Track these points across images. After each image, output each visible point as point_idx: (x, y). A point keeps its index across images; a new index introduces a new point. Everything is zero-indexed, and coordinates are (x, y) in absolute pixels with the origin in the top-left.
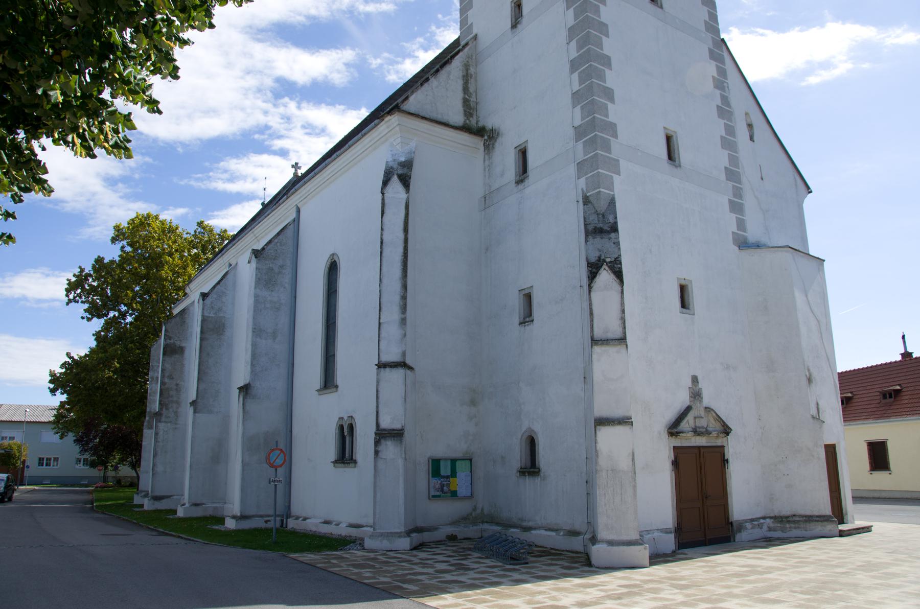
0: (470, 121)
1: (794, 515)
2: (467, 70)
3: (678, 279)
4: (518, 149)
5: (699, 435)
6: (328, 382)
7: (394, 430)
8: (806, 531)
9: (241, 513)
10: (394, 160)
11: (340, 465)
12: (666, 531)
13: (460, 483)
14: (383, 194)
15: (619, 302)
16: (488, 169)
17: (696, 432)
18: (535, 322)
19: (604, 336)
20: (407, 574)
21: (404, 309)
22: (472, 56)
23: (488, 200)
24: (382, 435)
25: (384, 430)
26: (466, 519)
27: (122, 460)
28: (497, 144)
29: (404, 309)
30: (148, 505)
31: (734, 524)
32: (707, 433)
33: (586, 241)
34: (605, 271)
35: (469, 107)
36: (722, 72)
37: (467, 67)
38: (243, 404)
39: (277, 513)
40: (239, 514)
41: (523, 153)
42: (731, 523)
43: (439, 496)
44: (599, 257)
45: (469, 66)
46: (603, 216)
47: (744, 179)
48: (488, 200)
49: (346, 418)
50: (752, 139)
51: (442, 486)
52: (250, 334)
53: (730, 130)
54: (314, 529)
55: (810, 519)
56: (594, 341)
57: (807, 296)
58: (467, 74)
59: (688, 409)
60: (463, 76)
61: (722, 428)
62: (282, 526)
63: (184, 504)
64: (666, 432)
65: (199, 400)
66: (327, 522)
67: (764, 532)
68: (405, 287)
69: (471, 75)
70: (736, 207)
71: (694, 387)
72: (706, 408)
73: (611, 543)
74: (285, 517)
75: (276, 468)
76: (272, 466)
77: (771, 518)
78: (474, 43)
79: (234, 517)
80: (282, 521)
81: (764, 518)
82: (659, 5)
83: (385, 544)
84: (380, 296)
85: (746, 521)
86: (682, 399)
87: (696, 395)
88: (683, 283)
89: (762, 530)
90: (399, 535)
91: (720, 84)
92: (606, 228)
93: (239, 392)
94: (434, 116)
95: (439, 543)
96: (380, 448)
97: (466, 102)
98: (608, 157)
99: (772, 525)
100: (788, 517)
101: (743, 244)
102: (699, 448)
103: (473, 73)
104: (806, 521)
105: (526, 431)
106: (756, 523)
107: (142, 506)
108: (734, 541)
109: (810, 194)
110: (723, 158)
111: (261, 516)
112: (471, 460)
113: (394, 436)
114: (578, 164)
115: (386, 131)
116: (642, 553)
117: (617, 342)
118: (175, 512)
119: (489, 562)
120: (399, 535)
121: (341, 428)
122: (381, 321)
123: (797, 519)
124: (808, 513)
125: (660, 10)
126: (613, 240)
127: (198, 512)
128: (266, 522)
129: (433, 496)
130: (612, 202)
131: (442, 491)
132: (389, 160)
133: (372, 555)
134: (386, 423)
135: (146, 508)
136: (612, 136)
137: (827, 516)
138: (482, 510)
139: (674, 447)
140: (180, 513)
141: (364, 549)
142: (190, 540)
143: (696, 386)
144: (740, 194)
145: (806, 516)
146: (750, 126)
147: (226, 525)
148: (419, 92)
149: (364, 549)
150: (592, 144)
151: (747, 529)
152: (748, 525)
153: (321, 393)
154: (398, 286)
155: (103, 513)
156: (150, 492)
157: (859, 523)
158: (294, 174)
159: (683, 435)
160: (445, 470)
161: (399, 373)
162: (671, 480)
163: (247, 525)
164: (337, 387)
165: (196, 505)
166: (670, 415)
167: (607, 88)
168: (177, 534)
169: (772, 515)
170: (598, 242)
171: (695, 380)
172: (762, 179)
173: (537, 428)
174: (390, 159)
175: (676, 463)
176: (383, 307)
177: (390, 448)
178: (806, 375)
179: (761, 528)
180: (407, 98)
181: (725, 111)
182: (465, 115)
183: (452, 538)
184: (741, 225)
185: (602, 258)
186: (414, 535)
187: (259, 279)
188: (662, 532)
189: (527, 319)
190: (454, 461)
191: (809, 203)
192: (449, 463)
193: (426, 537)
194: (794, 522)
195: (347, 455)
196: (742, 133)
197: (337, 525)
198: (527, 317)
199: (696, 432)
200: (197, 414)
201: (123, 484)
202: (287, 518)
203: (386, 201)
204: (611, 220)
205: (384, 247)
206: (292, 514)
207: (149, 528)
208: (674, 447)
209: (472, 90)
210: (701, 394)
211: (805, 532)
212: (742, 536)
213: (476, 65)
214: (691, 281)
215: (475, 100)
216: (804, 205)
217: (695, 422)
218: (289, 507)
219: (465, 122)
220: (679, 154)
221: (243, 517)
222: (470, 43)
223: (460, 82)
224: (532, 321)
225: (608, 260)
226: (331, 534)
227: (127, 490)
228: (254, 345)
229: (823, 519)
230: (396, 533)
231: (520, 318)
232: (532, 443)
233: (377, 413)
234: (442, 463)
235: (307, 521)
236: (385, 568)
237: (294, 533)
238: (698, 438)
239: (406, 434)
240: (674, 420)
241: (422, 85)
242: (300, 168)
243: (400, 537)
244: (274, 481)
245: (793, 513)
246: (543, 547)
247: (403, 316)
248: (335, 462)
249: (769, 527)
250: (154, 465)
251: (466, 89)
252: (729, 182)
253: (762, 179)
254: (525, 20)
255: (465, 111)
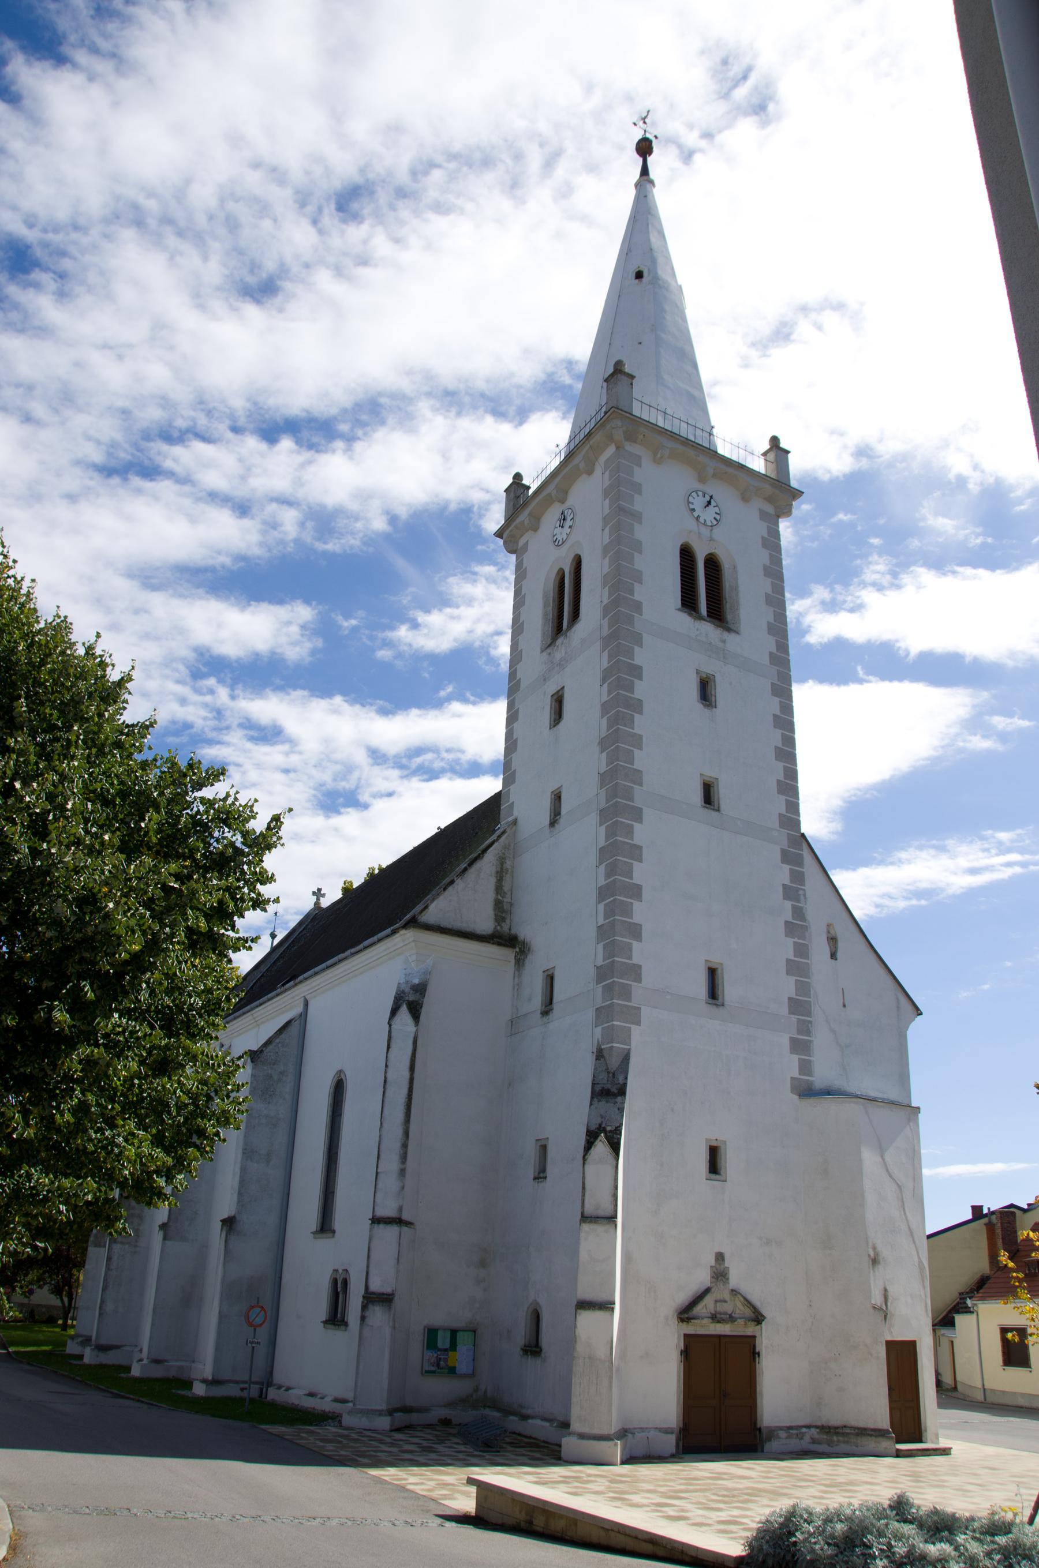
0: (502, 927)
1: (845, 1427)
2: (502, 864)
3: (707, 1140)
4: (547, 973)
5: (719, 1322)
6: (325, 1226)
7: (383, 1294)
8: (857, 1446)
9: (213, 1376)
10: (407, 982)
11: (330, 1326)
12: (667, 1431)
13: (461, 1359)
14: (390, 1026)
15: (613, 1178)
16: (517, 987)
17: (715, 1318)
18: (548, 1179)
19: (595, 1214)
20: (369, 1451)
21: (404, 1158)
22: (509, 845)
23: (515, 1025)
24: (371, 1298)
25: (373, 1293)
26: (464, 1402)
27: (40, 1281)
28: (527, 961)
29: (404, 1158)
30: (89, 1356)
31: (764, 1431)
32: (731, 1319)
33: (591, 1104)
34: (601, 1143)
35: (502, 910)
36: (798, 877)
37: (502, 860)
38: (226, 1241)
39: (253, 1379)
40: (210, 1378)
41: (550, 979)
42: (760, 1429)
43: (434, 1372)
44: (600, 1125)
45: (505, 858)
46: (614, 1074)
47: (815, 1009)
48: (515, 1025)
49: (340, 1271)
50: (833, 956)
51: (439, 1360)
52: (240, 1156)
53: (802, 950)
54: (296, 1402)
55: (863, 1432)
56: (585, 1218)
57: (882, 1157)
58: (502, 869)
59: (707, 1291)
60: (497, 872)
61: (752, 1315)
62: (260, 1396)
63: (141, 1360)
64: (675, 1317)
65: (170, 1224)
66: (311, 1394)
67: (805, 1444)
68: (406, 1133)
69: (507, 870)
70: (800, 1046)
71: (718, 1266)
72: (732, 1290)
73: (582, 1436)
74: (265, 1385)
75: (255, 1327)
76: (250, 1324)
77: (817, 1427)
78: (514, 828)
79: (204, 1381)
80: (261, 1390)
81: (808, 1427)
82: (716, 807)
83: (363, 1422)
84: (380, 1141)
85: (781, 1428)
86: (702, 1278)
87: (720, 1274)
88: (714, 1144)
89: (802, 1441)
90: (380, 1413)
91: (792, 892)
92: (614, 1090)
93: (222, 1225)
94: (458, 925)
95: (430, 1426)
96: (367, 1314)
97: (498, 904)
98: (626, 1006)
99: (816, 1436)
100: (837, 1428)
101: (807, 1091)
102: (720, 1336)
103: (508, 867)
104: (857, 1435)
105: (531, 1304)
106: (794, 1432)
107: (81, 1357)
108: (763, 1451)
109: (919, 1017)
110: (788, 986)
111: (237, 1382)
112: (475, 1332)
113: (383, 1302)
114: (597, 1009)
115: (402, 945)
116: (617, 1449)
117: (605, 1221)
118: (128, 1369)
119: (462, 1448)
120: (380, 1413)
121: (335, 1281)
122: (379, 1170)
123: (848, 1431)
124: (862, 1425)
125: (717, 813)
126: (618, 1105)
127: (158, 1372)
128: (242, 1389)
129: (427, 1372)
130: (626, 1058)
131: (438, 1366)
132: (401, 982)
133: (346, 1432)
134: (376, 1286)
135: (87, 1360)
136: (635, 981)
137: (884, 1430)
138: (486, 1391)
139: (685, 1335)
140: (136, 1371)
141: (341, 1426)
142: (152, 1405)
143: (720, 1264)
144: (809, 1029)
145: (859, 1429)
146: (833, 940)
147: (193, 1391)
148: (441, 898)
149: (341, 1426)
150: (609, 990)
151: (779, 1438)
152: (782, 1434)
153: (317, 1236)
154: (399, 1132)
155: (28, 1364)
156: (94, 1338)
157: (943, 1443)
158: (315, 904)
159: (696, 1321)
160: (443, 1341)
161: (393, 1231)
162: (679, 1373)
163: (219, 1392)
164: (334, 1232)
165: (157, 1361)
166: (682, 1298)
167: (634, 924)
168: (137, 1398)
169: (819, 1424)
170: (603, 1106)
171: (720, 1257)
172: (844, 1006)
173: (542, 1301)
174: (403, 981)
175: (686, 1353)
176: (382, 1155)
177: (378, 1315)
178: (869, 1256)
179: (802, 1438)
180: (426, 907)
181: (796, 927)
182: (496, 920)
183: (446, 1422)
184: (805, 1067)
185: (603, 1126)
186: (397, 1415)
187: (254, 1088)
188: (660, 1431)
189: (542, 1175)
190: (454, 1332)
191: (916, 1031)
192: (448, 1334)
193: (415, 1418)
194: (843, 1434)
195: (339, 1315)
196: (819, 948)
197: (322, 1398)
198: (541, 1175)
199: (715, 1318)
200: (166, 1242)
201: (37, 1317)
202: (268, 1387)
203: (393, 1034)
204: (621, 1081)
205: (388, 1086)
206: (275, 1382)
207: (99, 1388)
208: (685, 1335)
209: (506, 888)
210: (726, 1274)
211: (854, 1447)
212: (772, 1446)
213: (514, 858)
214: (725, 1142)
215: (509, 900)
216: (908, 1032)
217: (716, 1307)
218: (271, 1373)
219: (495, 928)
220: (723, 990)
221: (215, 1382)
222: (508, 831)
223: (493, 880)
224: (545, 1178)
225: (609, 1128)
226: (314, 1409)
227: (45, 1329)
228: (244, 1169)
229: (880, 1433)
230: (377, 1410)
231: (535, 1171)
232: (536, 1317)
233: (367, 1273)
234: (440, 1334)
235: (291, 1391)
236: (352, 1444)
237: (273, 1405)
238: (719, 1325)
239: (396, 1299)
240: (687, 1304)
241: (445, 889)
242: (323, 895)
243: (380, 1415)
244: (252, 1343)
245: (844, 1423)
246: (531, 1437)
247: (402, 1167)
248: (326, 1322)
249: (812, 1438)
250: (103, 1302)
251: (499, 888)
252: (792, 1016)
253: (844, 1006)
254: (563, 820)
255: (496, 915)
